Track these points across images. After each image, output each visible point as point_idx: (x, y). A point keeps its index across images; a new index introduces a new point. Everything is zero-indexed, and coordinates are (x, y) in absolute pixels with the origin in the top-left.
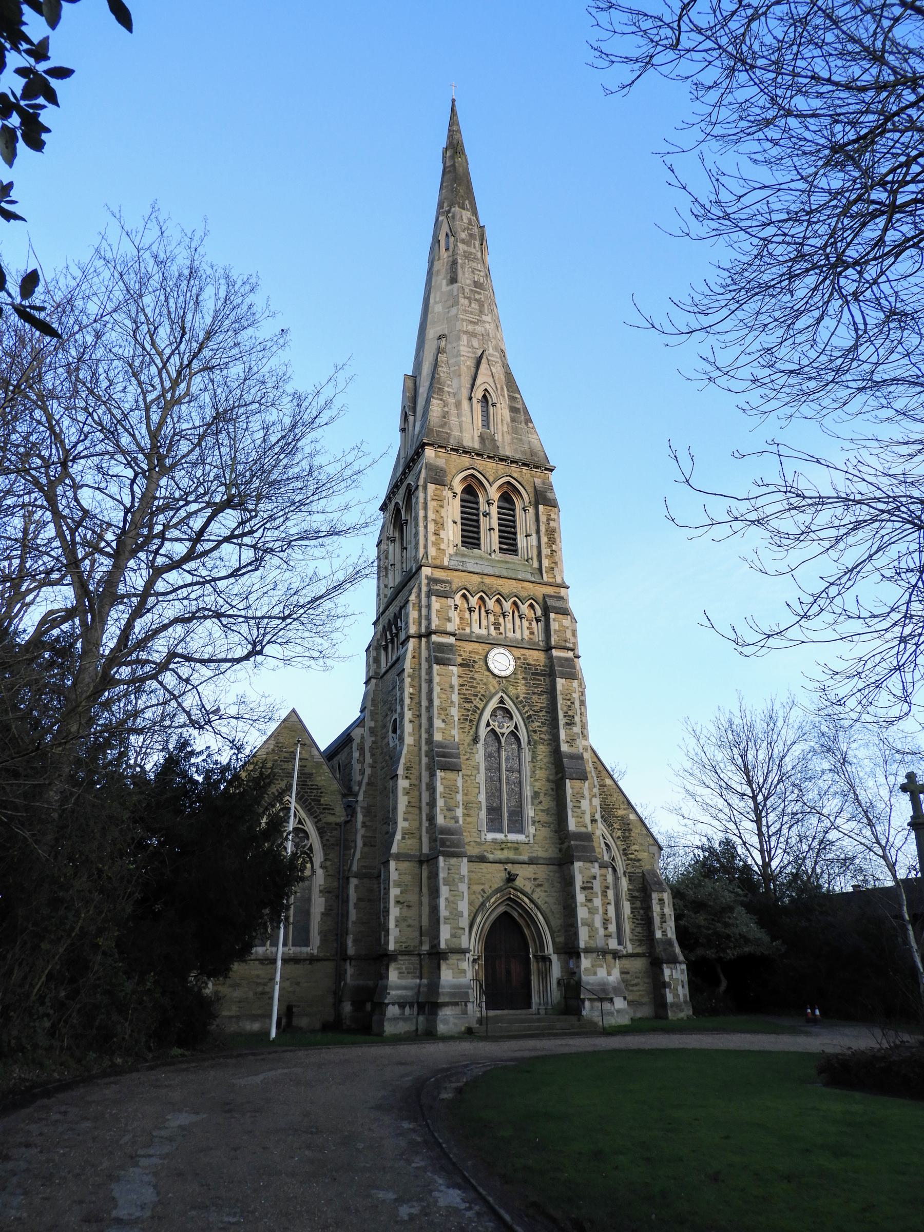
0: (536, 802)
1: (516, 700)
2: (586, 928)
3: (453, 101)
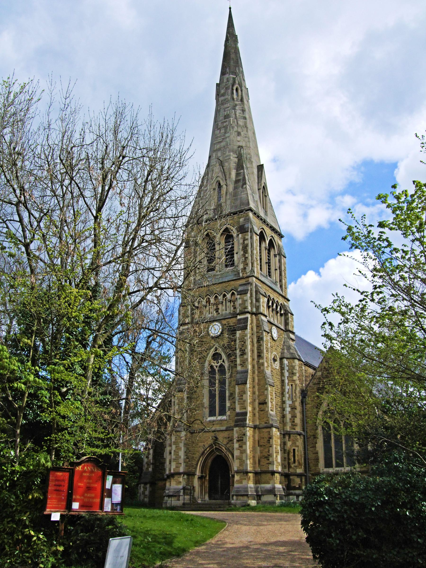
0: (231, 398)
1: (224, 348)
2: (238, 460)
3: (230, 8)
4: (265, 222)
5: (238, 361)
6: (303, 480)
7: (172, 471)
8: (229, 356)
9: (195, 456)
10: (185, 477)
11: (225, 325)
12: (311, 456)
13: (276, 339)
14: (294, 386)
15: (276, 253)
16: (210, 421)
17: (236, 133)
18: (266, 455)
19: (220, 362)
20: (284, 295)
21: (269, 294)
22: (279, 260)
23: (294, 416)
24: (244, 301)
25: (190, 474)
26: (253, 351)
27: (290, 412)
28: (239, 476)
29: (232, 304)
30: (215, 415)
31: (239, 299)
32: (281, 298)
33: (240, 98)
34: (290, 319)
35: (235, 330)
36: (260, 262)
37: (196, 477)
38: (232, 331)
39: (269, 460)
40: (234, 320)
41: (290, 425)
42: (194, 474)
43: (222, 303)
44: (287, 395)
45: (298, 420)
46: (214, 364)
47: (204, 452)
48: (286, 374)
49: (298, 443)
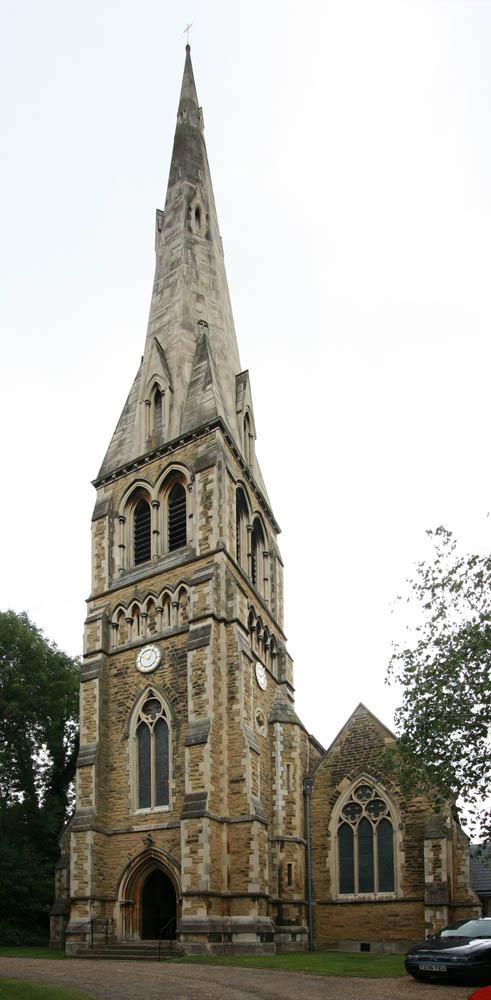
1: (164, 689)
3: (188, 48)
5: (191, 706)
6: (303, 911)
7: (72, 895)
8: (173, 703)
11: (168, 648)
12: (316, 875)
14: (292, 768)
15: (267, 550)
16: (140, 816)
17: (195, 296)
18: (243, 868)
22: (272, 565)
23: (291, 815)
24: (203, 597)
25: (106, 902)
27: (283, 808)
28: (190, 903)
29: (181, 610)
30: (149, 805)
33: (204, 233)
34: (287, 664)
37: (118, 904)
39: (247, 875)
41: (284, 828)
42: (114, 901)
43: (162, 611)
44: (280, 782)
45: (297, 821)
46: (146, 719)
47: (131, 863)
48: (279, 747)
49: (295, 856)
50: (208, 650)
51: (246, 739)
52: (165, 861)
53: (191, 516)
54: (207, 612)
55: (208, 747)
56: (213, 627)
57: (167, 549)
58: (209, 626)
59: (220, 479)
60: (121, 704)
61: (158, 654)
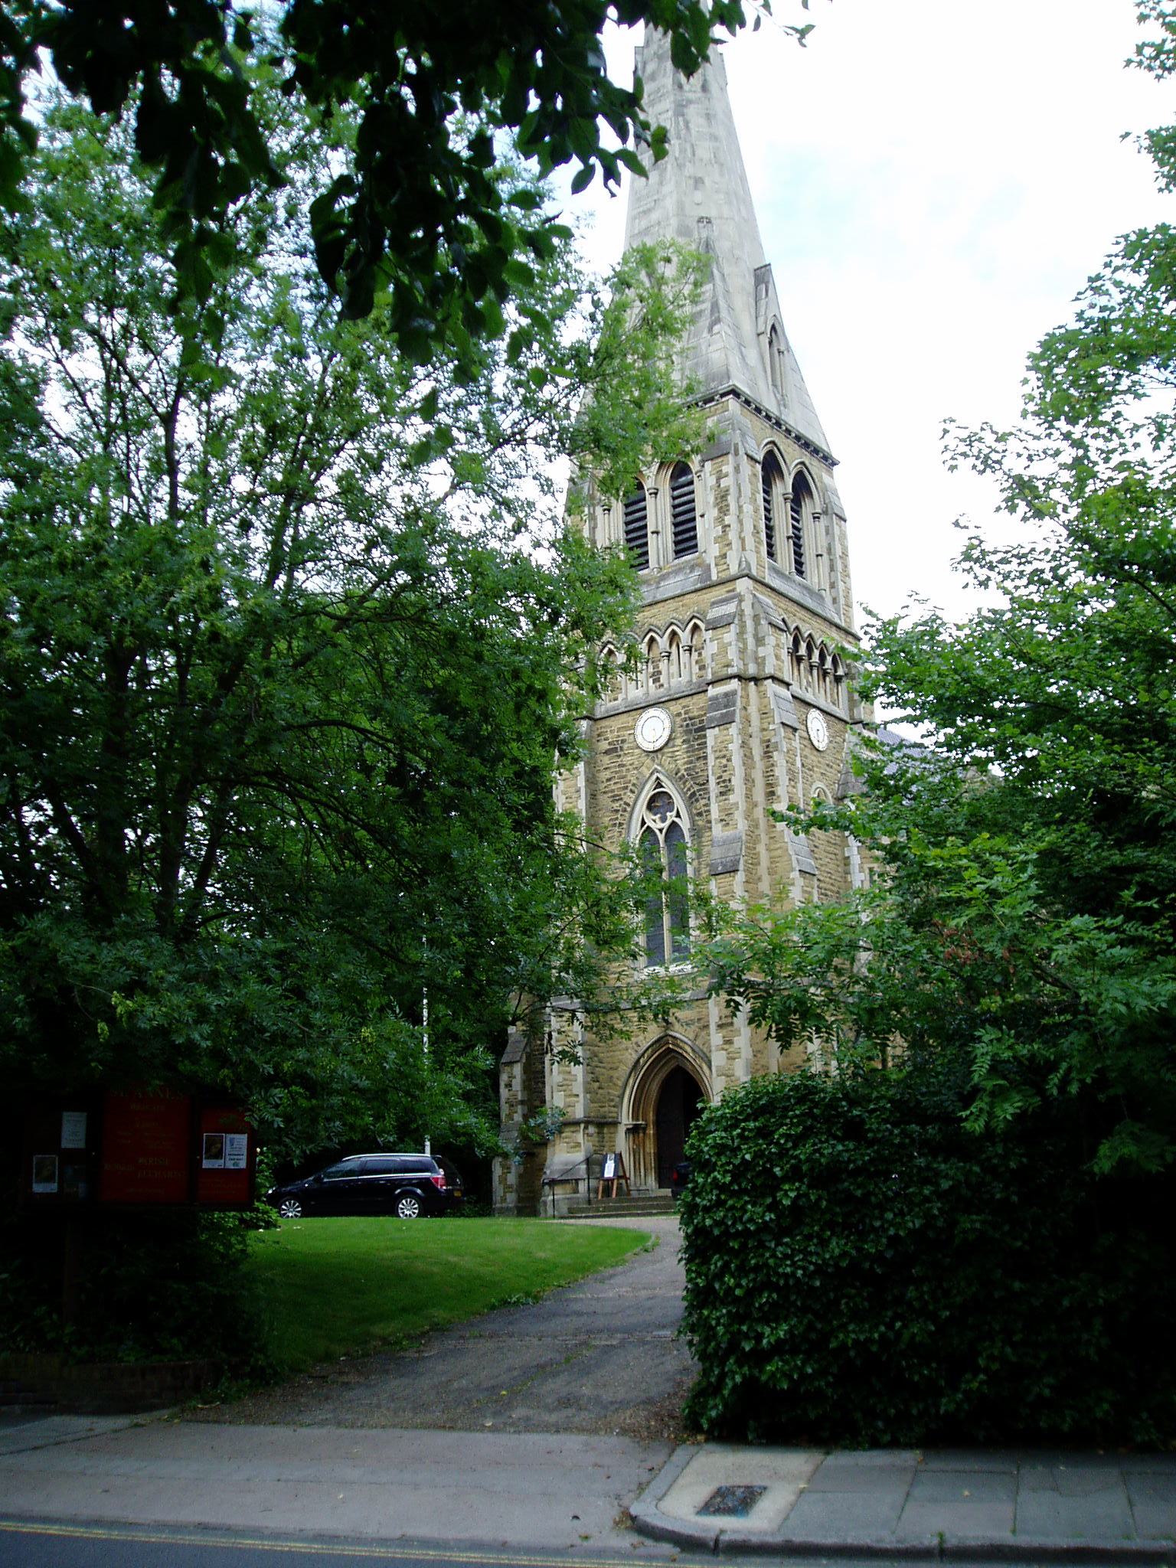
1: (677, 777)
4: (778, 424)
8: (691, 799)
9: (615, 1074)
10: (592, 1129)
11: (679, 714)
13: (821, 746)
17: (691, 182)
19: (671, 816)
20: (843, 625)
21: (798, 623)
24: (724, 648)
25: (603, 1124)
26: (748, 780)
29: (695, 655)
31: (711, 640)
32: (834, 633)
35: (703, 729)
36: (769, 537)
37: (622, 1129)
38: (697, 730)
40: (700, 701)
42: (615, 1124)
46: (656, 823)
47: (638, 1061)
50: (733, 729)
51: (794, 857)
52: (690, 1055)
53: (702, 516)
54: (731, 671)
55: (740, 877)
56: (739, 693)
57: (671, 554)
58: (734, 693)
59: (737, 469)
60: (616, 798)
61: (667, 724)
